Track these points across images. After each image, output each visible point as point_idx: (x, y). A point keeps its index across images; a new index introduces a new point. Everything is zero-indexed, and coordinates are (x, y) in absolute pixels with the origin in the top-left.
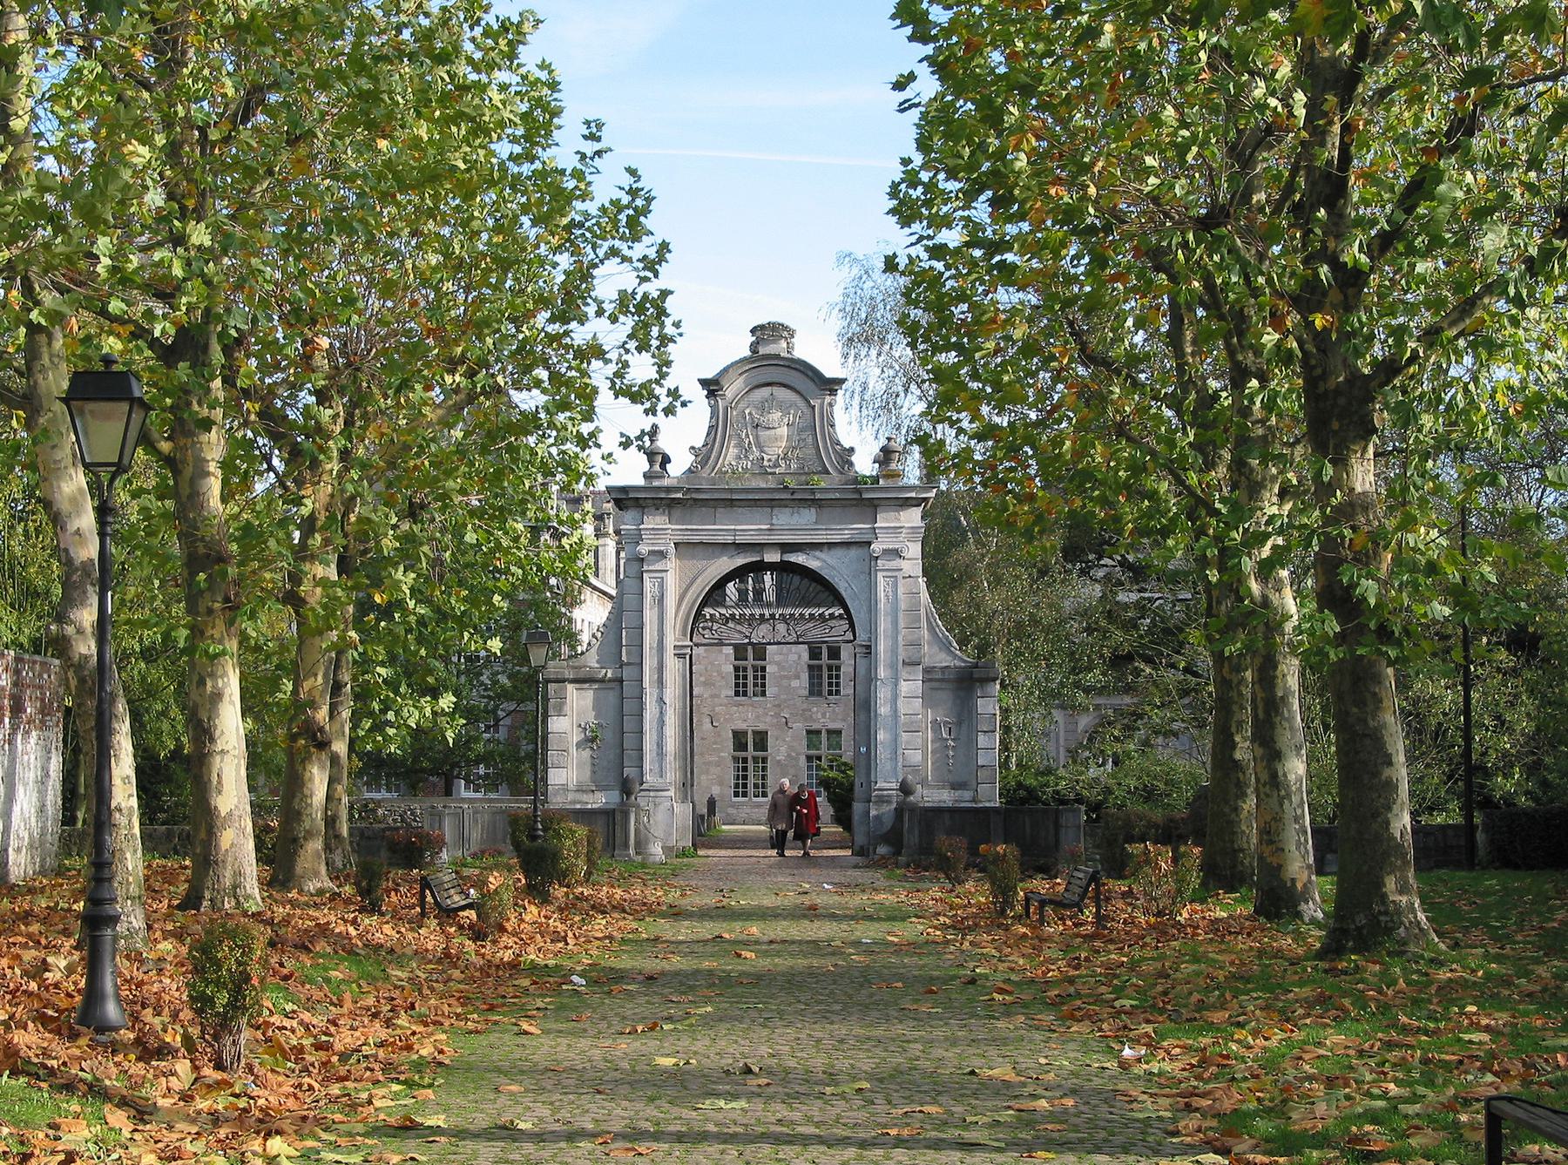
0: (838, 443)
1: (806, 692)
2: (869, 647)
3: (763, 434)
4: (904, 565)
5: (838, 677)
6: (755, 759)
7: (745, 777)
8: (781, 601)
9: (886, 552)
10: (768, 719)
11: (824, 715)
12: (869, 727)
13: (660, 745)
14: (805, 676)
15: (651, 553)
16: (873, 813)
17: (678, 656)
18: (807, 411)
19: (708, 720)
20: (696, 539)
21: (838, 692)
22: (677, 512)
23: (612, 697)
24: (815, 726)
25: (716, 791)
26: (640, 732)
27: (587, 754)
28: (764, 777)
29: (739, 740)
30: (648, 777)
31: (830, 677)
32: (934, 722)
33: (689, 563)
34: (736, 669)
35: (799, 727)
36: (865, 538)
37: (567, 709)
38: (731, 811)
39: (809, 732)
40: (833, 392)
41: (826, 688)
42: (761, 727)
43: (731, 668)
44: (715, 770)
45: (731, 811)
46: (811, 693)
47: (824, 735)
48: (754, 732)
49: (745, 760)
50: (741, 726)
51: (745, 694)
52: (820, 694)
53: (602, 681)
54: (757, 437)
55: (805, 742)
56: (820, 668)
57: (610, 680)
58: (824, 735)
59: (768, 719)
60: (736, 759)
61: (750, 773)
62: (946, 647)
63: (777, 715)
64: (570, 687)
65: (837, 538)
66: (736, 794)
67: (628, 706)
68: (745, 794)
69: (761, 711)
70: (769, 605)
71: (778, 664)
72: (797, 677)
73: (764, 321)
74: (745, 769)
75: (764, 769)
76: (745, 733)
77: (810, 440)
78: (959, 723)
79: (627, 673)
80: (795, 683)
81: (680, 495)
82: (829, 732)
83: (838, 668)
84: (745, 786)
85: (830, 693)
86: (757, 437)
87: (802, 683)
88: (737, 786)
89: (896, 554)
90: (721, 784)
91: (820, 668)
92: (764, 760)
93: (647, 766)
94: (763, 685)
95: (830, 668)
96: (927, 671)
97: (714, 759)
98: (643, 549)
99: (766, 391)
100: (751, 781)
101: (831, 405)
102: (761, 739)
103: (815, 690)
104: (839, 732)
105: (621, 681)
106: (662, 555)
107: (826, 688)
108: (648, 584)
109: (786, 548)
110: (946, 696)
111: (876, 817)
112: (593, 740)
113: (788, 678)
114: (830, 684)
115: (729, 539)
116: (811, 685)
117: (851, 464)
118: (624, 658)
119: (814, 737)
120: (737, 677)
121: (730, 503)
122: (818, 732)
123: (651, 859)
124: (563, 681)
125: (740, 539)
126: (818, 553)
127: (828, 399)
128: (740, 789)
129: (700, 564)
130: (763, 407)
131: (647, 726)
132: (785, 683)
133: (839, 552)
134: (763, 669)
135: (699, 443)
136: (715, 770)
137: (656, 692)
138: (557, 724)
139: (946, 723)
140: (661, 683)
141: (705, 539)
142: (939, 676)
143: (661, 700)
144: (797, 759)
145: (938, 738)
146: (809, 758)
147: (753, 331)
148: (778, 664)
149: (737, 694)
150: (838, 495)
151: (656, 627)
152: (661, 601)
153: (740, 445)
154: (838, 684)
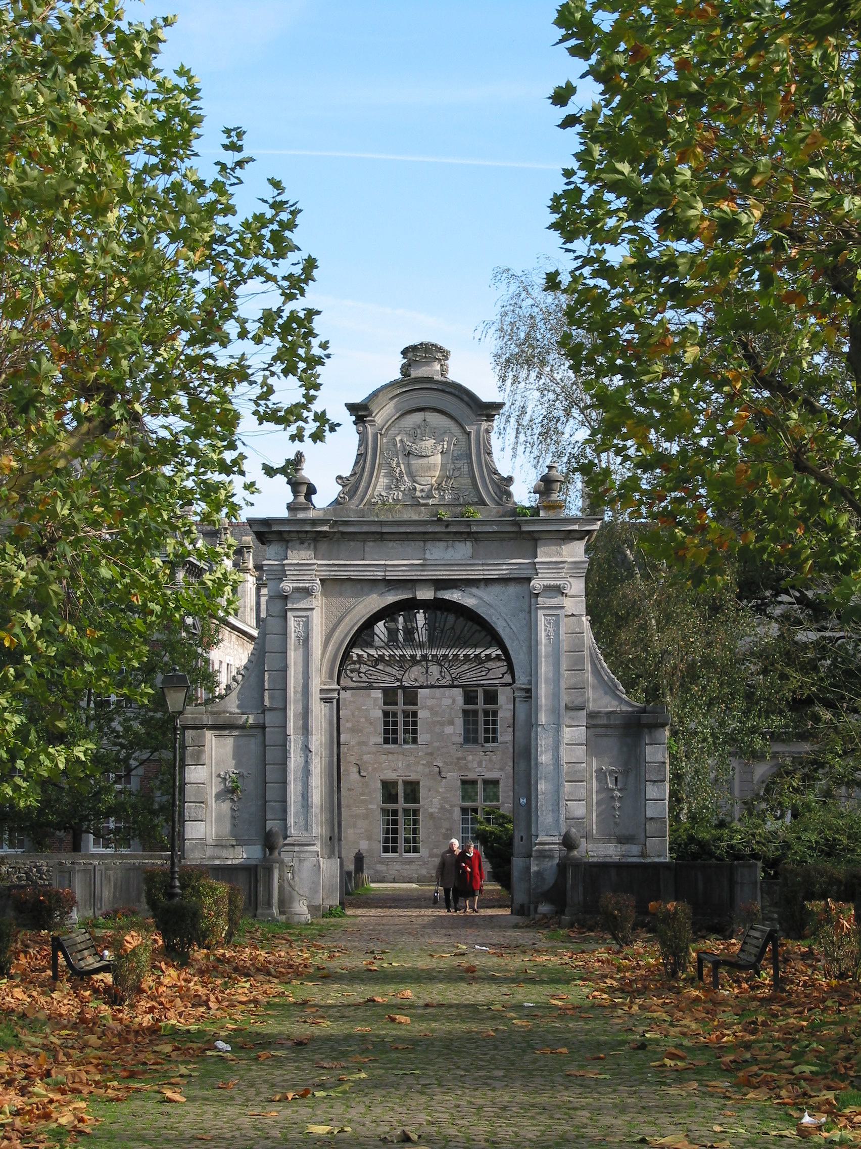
0: (496, 472)
1: (460, 739)
2: (528, 691)
3: (414, 462)
4: (567, 602)
5: (495, 722)
6: (406, 812)
7: (395, 831)
8: (433, 641)
9: (547, 588)
10: (420, 768)
11: (480, 764)
12: (529, 775)
13: (305, 796)
14: (459, 722)
15: (297, 590)
16: (534, 868)
17: (326, 700)
18: (463, 438)
19: (355, 769)
20: (343, 574)
21: (495, 740)
22: (323, 546)
23: (253, 745)
24: (471, 776)
25: (364, 846)
26: (284, 783)
27: (226, 806)
28: (415, 831)
29: (389, 791)
30: (292, 831)
31: (486, 723)
32: (599, 771)
33: (337, 601)
34: (386, 714)
35: (453, 777)
36: (525, 573)
37: (206, 757)
38: (380, 867)
39: (464, 782)
40: (490, 418)
41: (481, 735)
42: (413, 777)
43: (380, 714)
44: (362, 824)
45: (380, 867)
46: (467, 740)
47: (480, 786)
48: (406, 783)
49: (395, 813)
50: (391, 776)
51: (395, 741)
52: (475, 741)
53: (243, 727)
54: (408, 466)
55: (459, 793)
56: (475, 713)
57: (252, 727)
58: (480, 786)
59: (420, 768)
60: (385, 812)
61: (401, 827)
62: (611, 690)
63: (429, 764)
64: (209, 735)
65: (494, 574)
66: (386, 850)
67: (272, 754)
68: (395, 850)
69: (412, 759)
70: (421, 646)
71: (431, 709)
72: (451, 723)
73: (415, 341)
74: (395, 822)
75: (416, 822)
76: (394, 784)
77: (465, 469)
78: (626, 773)
79: (269, 718)
80: (449, 730)
81: (325, 528)
82: (486, 782)
83: (495, 713)
84: (395, 840)
85: (487, 740)
86: (408, 466)
87: (456, 729)
88: (386, 840)
89: (558, 591)
90: (369, 838)
91: (475, 713)
92: (416, 812)
93: (291, 820)
94: (415, 732)
95: (486, 713)
96: (592, 715)
97: (361, 811)
98: (287, 586)
99: (417, 417)
100: (401, 835)
101: (488, 432)
102: (412, 791)
103: (470, 737)
104: (495, 783)
105: (263, 727)
106: (307, 592)
107: (481, 735)
108: (292, 622)
109: (441, 584)
110: (611, 743)
111: (538, 873)
112: (233, 791)
113: (442, 724)
114: (486, 731)
115: (379, 575)
116: (467, 731)
117: (509, 495)
118: (267, 703)
119: (469, 788)
120: (386, 723)
121: (381, 537)
122: (474, 783)
123: (296, 919)
124: (201, 727)
125: (391, 575)
126: (474, 590)
127: (484, 425)
128: (390, 845)
129: (349, 602)
130: (415, 434)
131: (291, 777)
132: (437, 729)
133: (496, 589)
134: (415, 714)
135: (346, 473)
136: (362, 824)
137: (300, 739)
138: (195, 774)
139: (612, 772)
140: (306, 730)
141: (354, 575)
142: (603, 721)
143: (306, 749)
144: (451, 812)
145: (603, 788)
146: (464, 811)
147: (405, 352)
148: (431, 709)
149: (386, 741)
150: (495, 528)
151: (300, 669)
152: (305, 641)
153: (390, 474)
154: (495, 731)
